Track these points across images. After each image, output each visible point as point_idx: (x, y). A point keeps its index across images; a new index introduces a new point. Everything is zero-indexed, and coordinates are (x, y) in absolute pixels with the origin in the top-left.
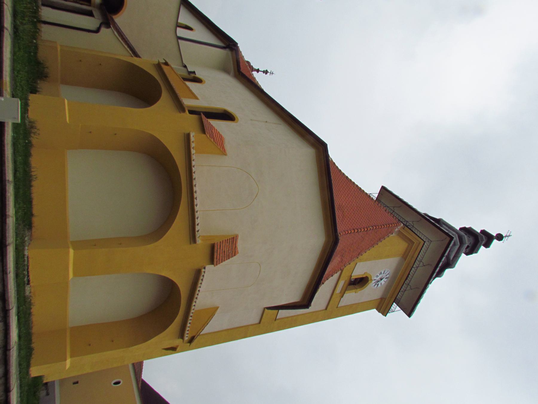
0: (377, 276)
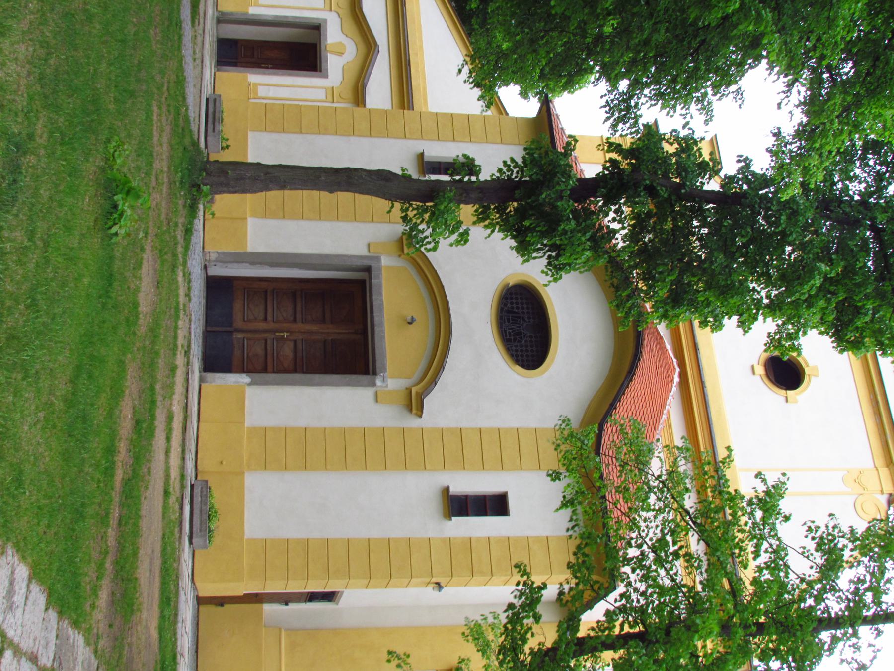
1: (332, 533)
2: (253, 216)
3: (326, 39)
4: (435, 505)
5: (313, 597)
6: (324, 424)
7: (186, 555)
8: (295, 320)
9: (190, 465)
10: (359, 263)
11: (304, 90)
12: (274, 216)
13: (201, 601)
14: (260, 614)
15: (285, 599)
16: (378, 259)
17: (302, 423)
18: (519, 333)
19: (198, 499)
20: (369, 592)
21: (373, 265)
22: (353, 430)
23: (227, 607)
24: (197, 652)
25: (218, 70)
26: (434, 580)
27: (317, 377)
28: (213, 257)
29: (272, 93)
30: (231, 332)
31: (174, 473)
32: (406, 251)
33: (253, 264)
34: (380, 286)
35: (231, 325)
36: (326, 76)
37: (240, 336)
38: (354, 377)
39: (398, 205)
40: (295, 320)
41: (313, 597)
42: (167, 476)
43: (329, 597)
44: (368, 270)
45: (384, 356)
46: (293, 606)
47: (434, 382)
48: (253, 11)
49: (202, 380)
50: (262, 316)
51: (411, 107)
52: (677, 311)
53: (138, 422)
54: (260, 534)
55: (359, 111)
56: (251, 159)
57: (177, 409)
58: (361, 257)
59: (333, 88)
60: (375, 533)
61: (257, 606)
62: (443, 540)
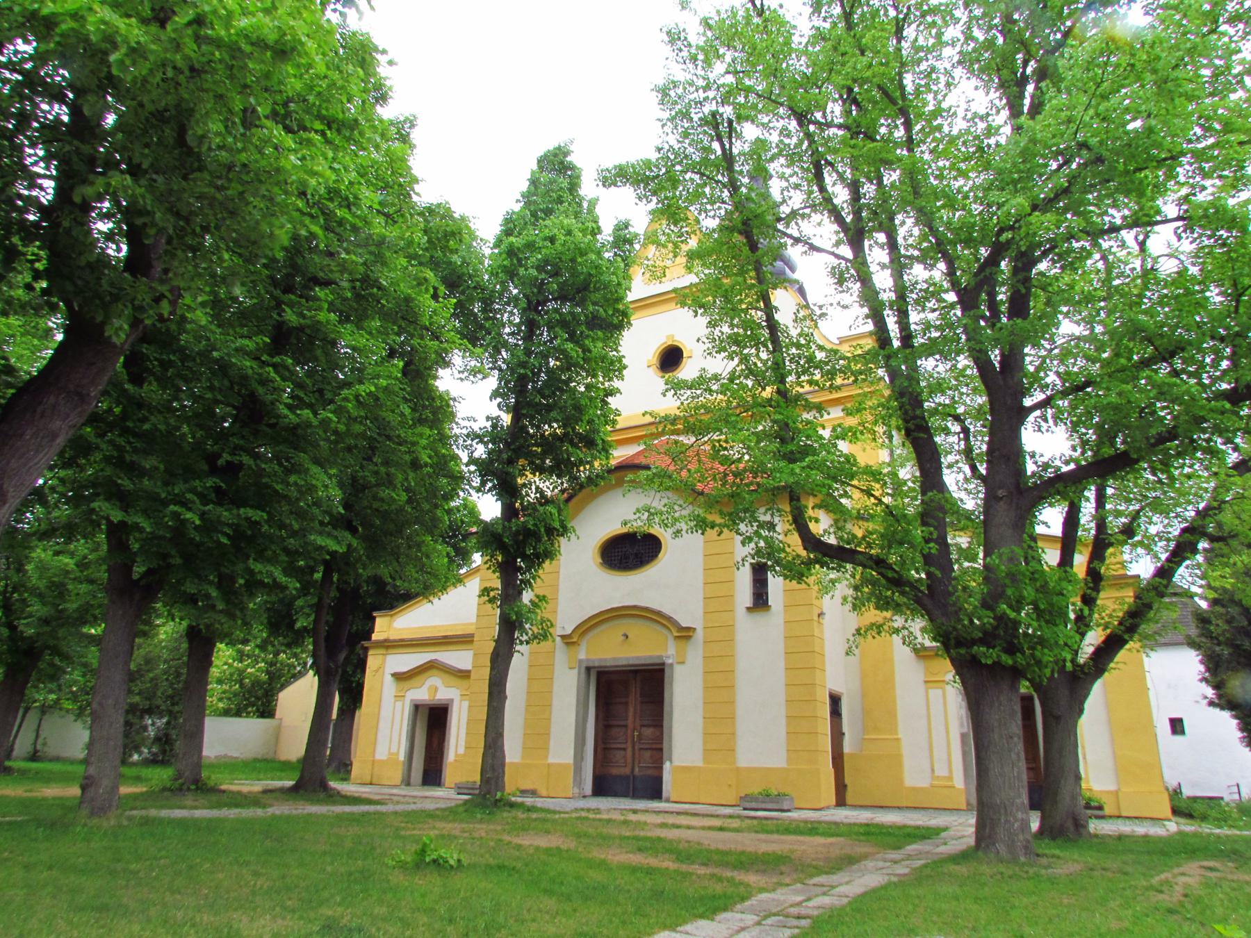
1: (782, 698)
2: (546, 757)
4: (760, 618)
5: (836, 712)
6: (700, 704)
7: (794, 815)
8: (626, 726)
9: (728, 811)
10: (583, 676)
12: (547, 742)
13: (841, 802)
14: (851, 755)
15: (837, 736)
16: (580, 661)
17: (700, 721)
18: (636, 555)
19: (754, 805)
20: (828, 668)
21: (584, 665)
22: (705, 681)
23: (847, 781)
24: (882, 807)
26: (816, 618)
27: (666, 708)
28: (576, 790)
29: (462, 743)
30: (634, 777)
31: (735, 823)
32: (575, 640)
33: (582, 759)
34: (601, 660)
35: (627, 777)
36: (452, 700)
37: (637, 770)
38: (666, 680)
39: (518, 648)
40: (626, 726)
41: (836, 712)
43: (835, 700)
44: (588, 669)
45: (651, 657)
46: (845, 729)
47: (670, 619)
48: (402, 757)
49: (668, 801)
50: (622, 752)
51: (472, 636)
52: (599, 442)
53: (640, 850)
54: (783, 755)
55: (473, 675)
56: (571, 761)
57: (659, 819)
58: (579, 674)
59: (926, 682)
60: (781, 664)
61: (845, 758)
62: (786, 611)
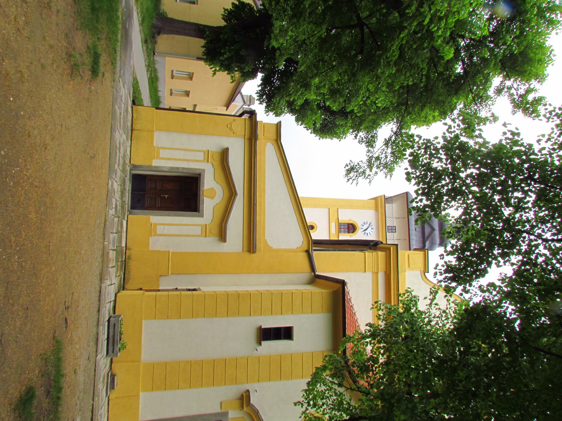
0: (363, 226)
3: (204, 186)
11: (187, 227)
12: (159, 389)
25: (130, 214)
36: (202, 216)
42: (119, 152)
